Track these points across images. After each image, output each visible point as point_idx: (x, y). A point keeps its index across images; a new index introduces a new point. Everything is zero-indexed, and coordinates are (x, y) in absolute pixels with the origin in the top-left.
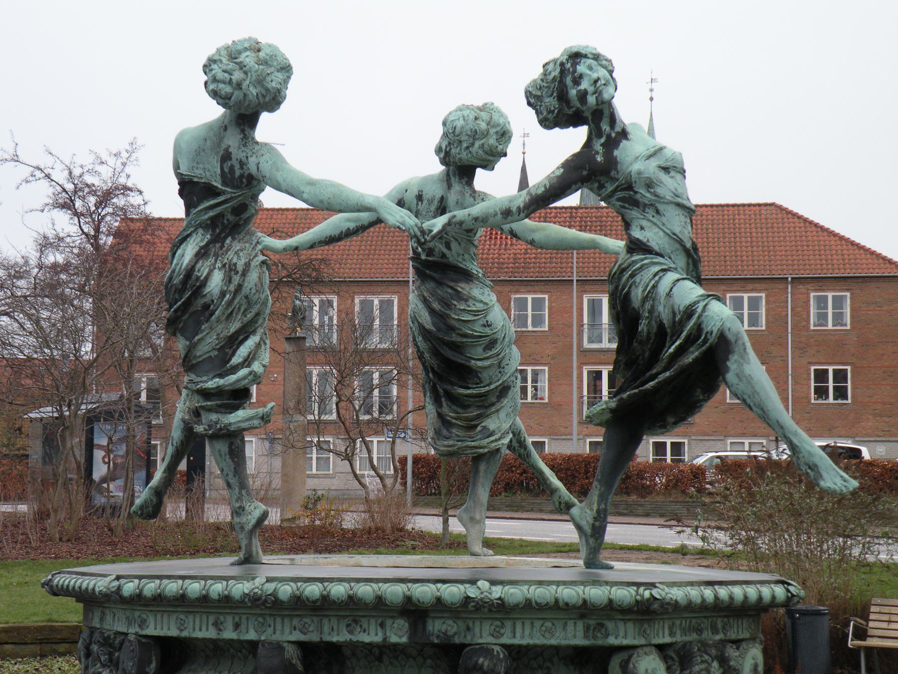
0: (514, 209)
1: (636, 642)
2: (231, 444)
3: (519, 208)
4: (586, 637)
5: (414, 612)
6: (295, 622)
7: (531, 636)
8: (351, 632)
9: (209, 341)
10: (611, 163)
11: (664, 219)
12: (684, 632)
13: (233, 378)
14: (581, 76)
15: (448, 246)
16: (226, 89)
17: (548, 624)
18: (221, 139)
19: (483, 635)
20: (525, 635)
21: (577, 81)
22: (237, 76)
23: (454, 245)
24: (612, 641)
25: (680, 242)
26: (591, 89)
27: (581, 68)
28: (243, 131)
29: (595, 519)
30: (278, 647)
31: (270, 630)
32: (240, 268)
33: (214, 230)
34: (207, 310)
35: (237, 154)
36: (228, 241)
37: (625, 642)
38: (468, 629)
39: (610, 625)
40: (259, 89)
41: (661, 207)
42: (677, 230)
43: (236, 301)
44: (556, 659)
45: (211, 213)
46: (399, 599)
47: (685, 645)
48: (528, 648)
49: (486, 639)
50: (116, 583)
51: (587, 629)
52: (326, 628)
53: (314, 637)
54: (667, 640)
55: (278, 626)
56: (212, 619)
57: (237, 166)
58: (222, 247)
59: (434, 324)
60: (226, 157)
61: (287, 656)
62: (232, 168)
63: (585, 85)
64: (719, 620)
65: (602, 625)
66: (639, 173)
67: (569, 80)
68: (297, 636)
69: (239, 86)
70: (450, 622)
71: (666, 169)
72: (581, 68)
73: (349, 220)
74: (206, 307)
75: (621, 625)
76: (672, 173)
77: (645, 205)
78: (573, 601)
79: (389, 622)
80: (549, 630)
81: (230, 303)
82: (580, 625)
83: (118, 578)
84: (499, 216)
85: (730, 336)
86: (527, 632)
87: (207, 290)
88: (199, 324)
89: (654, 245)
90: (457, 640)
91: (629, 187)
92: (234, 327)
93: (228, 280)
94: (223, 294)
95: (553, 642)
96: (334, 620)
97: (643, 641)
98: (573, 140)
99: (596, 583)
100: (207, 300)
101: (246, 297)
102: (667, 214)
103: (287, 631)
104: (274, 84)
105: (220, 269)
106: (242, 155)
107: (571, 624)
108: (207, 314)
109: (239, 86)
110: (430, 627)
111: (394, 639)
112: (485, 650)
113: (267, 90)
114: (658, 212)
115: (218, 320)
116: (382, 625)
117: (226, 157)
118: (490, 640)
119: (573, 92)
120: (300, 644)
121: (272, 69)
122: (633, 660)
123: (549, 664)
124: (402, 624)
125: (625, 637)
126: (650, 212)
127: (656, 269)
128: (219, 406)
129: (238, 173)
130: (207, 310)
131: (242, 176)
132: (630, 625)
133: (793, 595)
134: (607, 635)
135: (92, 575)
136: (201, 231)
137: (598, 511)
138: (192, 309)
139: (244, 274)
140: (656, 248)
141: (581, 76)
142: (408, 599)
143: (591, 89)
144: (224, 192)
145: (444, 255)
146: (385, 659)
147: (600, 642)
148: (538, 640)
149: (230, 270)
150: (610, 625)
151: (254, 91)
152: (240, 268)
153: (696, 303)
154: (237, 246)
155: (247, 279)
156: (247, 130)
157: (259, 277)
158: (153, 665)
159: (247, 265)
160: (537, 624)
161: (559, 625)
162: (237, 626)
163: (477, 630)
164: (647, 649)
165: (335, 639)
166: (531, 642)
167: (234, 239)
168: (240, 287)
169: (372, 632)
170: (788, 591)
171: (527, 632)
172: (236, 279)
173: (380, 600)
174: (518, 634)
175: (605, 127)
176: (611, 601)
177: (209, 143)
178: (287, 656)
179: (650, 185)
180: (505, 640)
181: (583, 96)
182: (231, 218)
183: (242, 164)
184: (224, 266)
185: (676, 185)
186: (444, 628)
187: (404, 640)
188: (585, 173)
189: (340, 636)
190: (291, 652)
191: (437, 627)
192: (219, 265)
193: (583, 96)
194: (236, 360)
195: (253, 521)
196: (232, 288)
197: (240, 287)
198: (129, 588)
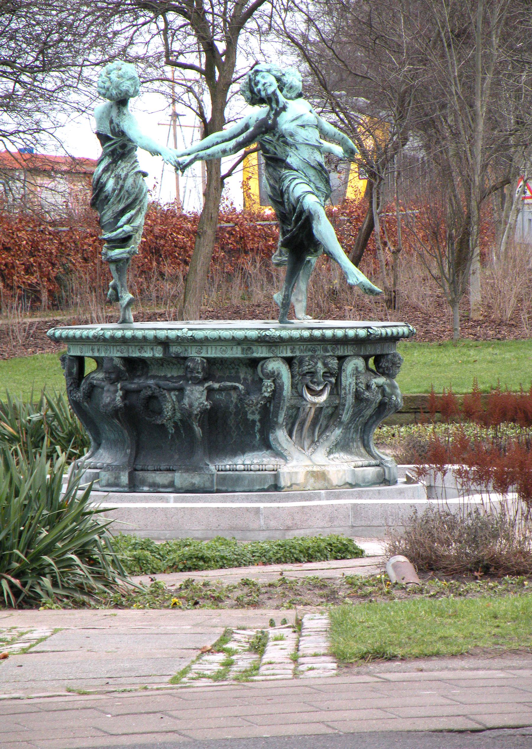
0: (228, 149)
1: (267, 356)
2: (117, 265)
3: (230, 149)
4: (243, 354)
5: (165, 343)
6: (118, 348)
7: (215, 353)
8: (140, 352)
9: (108, 215)
10: (275, 124)
11: (299, 152)
12: (301, 351)
13: (115, 233)
14: (258, 82)
15: (276, 149)
16: (103, 91)
17: (224, 348)
18: (110, 112)
19: (192, 352)
20: (213, 353)
21: (256, 84)
22: (108, 84)
23: (278, 147)
24: (255, 355)
25: (308, 163)
26: (262, 88)
27: (258, 78)
28: (119, 108)
29: (283, 299)
30: (111, 359)
31: (109, 352)
32: (123, 177)
33: (113, 157)
34: (107, 199)
35: (116, 121)
36: (119, 162)
37: (262, 355)
38: (186, 350)
39: (254, 348)
40: (117, 91)
41: (298, 146)
42: (306, 157)
43: (122, 193)
44: (241, 365)
45: (110, 149)
46: (174, 337)
47: (301, 356)
48: (215, 359)
49: (194, 354)
50: (102, 332)
51: (243, 349)
52: (130, 351)
53: (126, 355)
54: (289, 354)
55: (112, 350)
56: (90, 347)
57: (116, 127)
58: (116, 165)
59: (271, 192)
60: (111, 122)
61: (114, 363)
62: (114, 127)
63: (260, 86)
64: (329, 346)
65: (250, 348)
66: (285, 130)
67: (253, 83)
68: (119, 354)
69: (108, 89)
70: (179, 347)
71: (303, 126)
72: (258, 78)
73: (218, 137)
74: (106, 197)
75: (260, 348)
76: (307, 128)
77: (291, 145)
78: (228, 337)
79: (155, 348)
80: (224, 351)
81: (118, 195)
82: (239, 348)
83: (102, 329)
84: (220, 153)
85: (312, 212)
86: (213, 352)
87: (106, 189)
88: (103, 206)
89: (295, 166)
90: (182, 355)
91: (284, 136)
92: (121, 206)
93: (117, 183)
94: (114, 190)
95: (226, 356)
96: (133, 347)
97: (271, 355)
98: (259, 112)
99: (284, 328)
100: (106, 193)
101: (127, 191)
102: (301, 149)
103: (115, 352)
104: (124, 88)
105: (113, 178)
106: (117, 121)
107: (235, 347)
108: (106, 201)
109: (108, 89)
110: (171, 350)
111: (157, 355)
112: (193, 359)
113: (121, 90)
114: (297, 148)
115: (113, 203)
116: (152, 349)
117: (111, 122)
118: (196, 355)
119: (255, 89)
120: (122, 358)
121: (124, 80)
122: (266, 364)
123: (237, 367)
124: (160, 348)
125: (237, 353)
126: (294, 148)
127: (291, 178)
128: (111, 247)
129: (117, 130)
130: (107, 199)
131: (119, 131)
132: (264, 348)
133: (371, 334)
134: (253, 353)
135: (76, 329)
136: (107, 157)
137: (284, 296)
138: (100, 198)
139: (124, 180)
140: (295, 167)
141: (258, 82)
142: (155, 337)
143: (262, 88)
144: (112, 139)
145: (275, 154)
146: (164, 365)
147: (249, 356)
148: (219, 355)
149: (118, 177)
150: (254, 348)
151: (114, 92)
152: (123, 177)
153: (301, 196)
154: (123, 165)
155: (126, 182)
156: (121, 107)
157: (134, 181)
158: (75, 369)
159: (127, 175)
160: (219, 348)
161: (229, 348)
162: (98, 350)
163: (189, 350)
164: (275, 359)
165: (134, 356)
166: (216, 356)
167: (122, 161)
168: (122, 186)
169: (148, 352)
170: (368, 331)
171: (213, 352)
172: (121, 182)
173: (145, 338)
174: (209, 353)
175: (274, 106)
176: (246, 337)
177: (105, 115)
178: (114, 363)
179: (291, 135)
180: (203, 355)
181: (259, 91)
182: (120, 151)
183: (118, 125)
184: (115, 176)
185: (308, 134)
186: (177, 350)
187: (161, 355)
188: (264, 129)
189: (136, 354)
190: (117, 362)
191: (174, 350)
192: (113, 175)
193: (259, 91)
194: (120, 224)
195: (126, 303)
196: (119, 187)
197: (122, 186)
198: (108, 334)
